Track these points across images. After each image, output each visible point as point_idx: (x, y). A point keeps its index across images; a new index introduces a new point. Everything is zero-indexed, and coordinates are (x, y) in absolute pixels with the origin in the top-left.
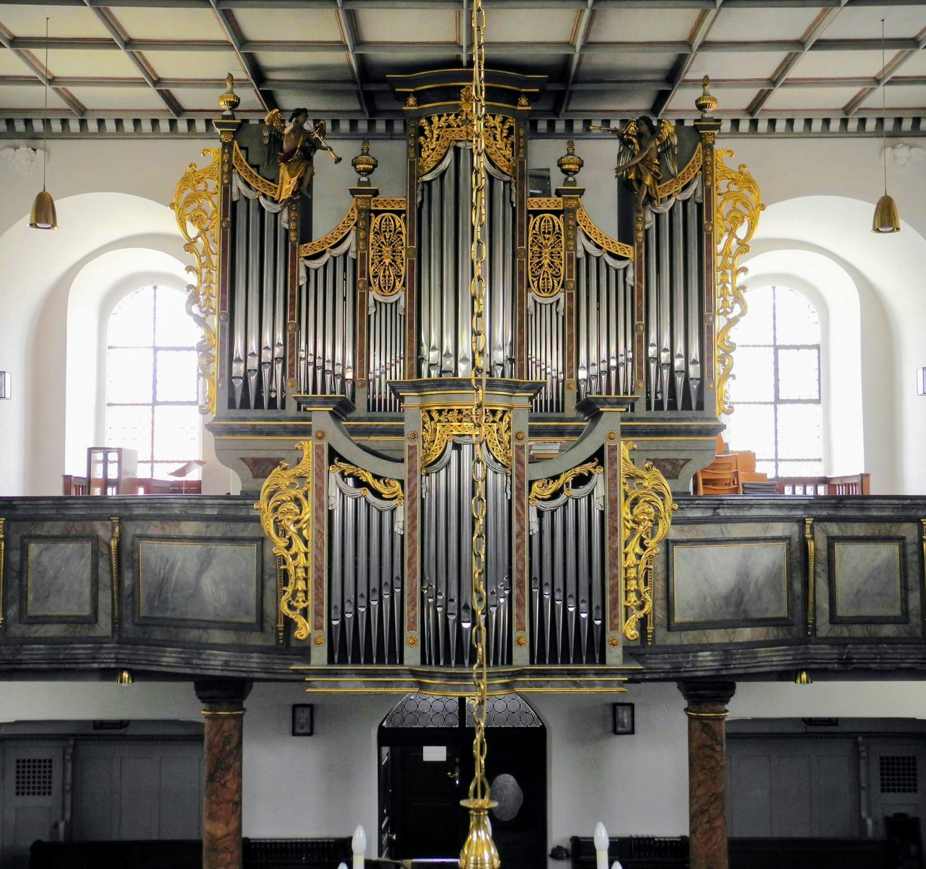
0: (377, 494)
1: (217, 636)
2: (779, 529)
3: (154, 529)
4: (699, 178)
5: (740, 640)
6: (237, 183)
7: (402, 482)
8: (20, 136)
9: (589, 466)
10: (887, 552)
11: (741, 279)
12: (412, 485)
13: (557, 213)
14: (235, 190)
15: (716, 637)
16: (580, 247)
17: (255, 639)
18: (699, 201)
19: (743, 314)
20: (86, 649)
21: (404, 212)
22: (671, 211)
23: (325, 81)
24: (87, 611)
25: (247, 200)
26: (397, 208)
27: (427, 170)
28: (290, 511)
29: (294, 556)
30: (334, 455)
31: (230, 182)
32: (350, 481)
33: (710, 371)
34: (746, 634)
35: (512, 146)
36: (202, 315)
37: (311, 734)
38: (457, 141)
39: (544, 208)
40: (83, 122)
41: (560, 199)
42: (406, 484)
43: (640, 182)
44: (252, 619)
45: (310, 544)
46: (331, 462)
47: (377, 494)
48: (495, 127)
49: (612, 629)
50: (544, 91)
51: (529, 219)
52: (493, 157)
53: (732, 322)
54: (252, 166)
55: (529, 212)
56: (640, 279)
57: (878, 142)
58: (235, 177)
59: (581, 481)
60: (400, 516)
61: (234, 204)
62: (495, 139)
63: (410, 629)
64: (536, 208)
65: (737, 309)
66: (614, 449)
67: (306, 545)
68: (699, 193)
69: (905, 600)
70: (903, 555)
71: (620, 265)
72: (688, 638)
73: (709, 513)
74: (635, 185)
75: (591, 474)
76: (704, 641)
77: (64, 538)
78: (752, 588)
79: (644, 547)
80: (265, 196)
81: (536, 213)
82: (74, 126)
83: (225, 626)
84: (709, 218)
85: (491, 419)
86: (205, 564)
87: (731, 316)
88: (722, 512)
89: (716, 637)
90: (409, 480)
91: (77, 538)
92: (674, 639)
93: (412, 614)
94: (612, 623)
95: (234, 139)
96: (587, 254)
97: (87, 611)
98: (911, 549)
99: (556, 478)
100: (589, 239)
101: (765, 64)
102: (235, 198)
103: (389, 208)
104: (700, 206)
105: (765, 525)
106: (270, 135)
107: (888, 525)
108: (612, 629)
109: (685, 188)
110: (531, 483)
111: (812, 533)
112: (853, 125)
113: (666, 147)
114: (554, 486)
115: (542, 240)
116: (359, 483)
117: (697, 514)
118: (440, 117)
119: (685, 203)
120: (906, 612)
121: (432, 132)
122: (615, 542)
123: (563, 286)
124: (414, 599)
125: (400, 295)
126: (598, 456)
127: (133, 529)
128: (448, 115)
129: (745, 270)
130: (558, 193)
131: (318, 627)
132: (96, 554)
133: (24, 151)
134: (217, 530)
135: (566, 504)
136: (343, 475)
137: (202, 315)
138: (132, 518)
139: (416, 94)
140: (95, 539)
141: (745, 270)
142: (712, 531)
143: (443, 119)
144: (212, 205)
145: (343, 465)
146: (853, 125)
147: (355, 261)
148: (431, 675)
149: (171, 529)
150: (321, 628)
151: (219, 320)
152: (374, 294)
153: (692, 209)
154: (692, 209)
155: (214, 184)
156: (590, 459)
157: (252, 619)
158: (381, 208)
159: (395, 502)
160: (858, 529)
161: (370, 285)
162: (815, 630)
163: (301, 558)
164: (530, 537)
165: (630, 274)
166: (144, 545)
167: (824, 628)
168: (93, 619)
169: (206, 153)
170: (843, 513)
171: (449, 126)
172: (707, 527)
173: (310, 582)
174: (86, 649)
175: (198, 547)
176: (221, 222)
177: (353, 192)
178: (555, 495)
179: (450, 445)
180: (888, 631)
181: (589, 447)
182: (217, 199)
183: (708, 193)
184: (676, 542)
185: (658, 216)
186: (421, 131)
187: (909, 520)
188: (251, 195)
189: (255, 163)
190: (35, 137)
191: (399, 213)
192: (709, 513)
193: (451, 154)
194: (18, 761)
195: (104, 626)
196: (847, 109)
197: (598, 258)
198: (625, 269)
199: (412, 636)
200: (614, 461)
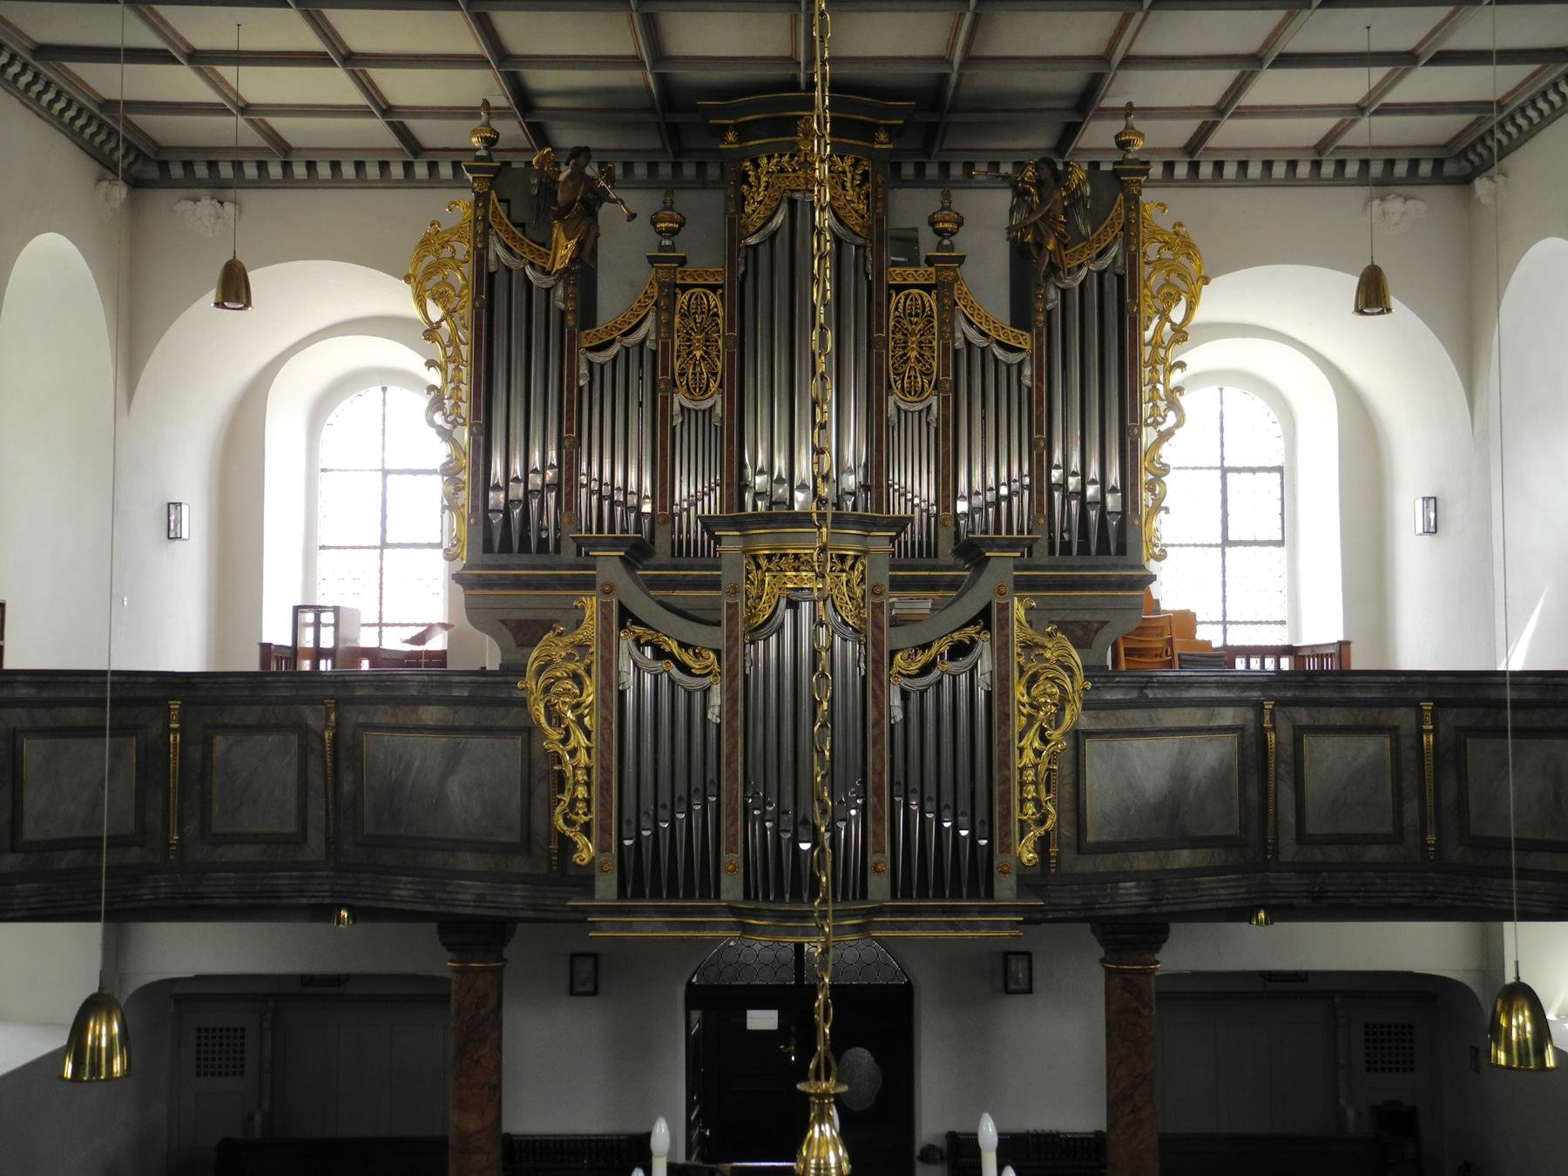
0: (685, 668)
1: (469, 861)
2: (1227, 716)
3: (382, 716)
4: (1120, 240)
5: (1176, 867)
6: (496, 249)
7: (718, 652)
8: (201, 184)
9: (971, 631)
10: (1373, 747)
11: (1176, 377)
12: (732, 656)
13: (928, 288)
14: (492, 257)
15: (1143, 861)
16: (958, 335)
17: (519, 865)
18: (1119, 272)
19: (1179, 424)
20: (291, 878)
21: (721, 286)
22: (1082, 285)
23: (614, 110)
24: (291, 827)
25: (509, 270)
26: (711, 281)
27: (752, 229)
28: (567, 692)
29: (573, 753)
30: (626, 617)
31: (486, 246)
32: (648, 651)
33: (1135, 502)
34: (1184, 858)
35: (867, 198)
36: (448, 427)
37: (595, 993)
38: (793, 191)
39: (910, 281)
40: (287, 166)
41: (931, 269)
42: (724, 655)
43: (1040, 246)
44: (514, 837)
45: (593, 736)
46: (622, 626)
47: (685, 668)
48: (844, 172)
49: (1002, 852)
50: (909, 124)
51: (890, 296)
52: (841, 213)
53: (1164, 436)
54: (516, 225)
55: (891, 287)
56: (1040, 379)
57: (1362, 192)
58: (493, 239)
59: (959, 650)
60: (716, 699)
61: (491, 276)
62: (844, 188)
63: (729, 851)
64: (899, 281)
65: (1171, 418)
66: (1005, 608)
67: (589, 738)
68: (1120, 261)
69: (1398, 812)
70: (1396, 750)
71: (1014, 358)
72: (1106, 863)
73: (1134, 694)
74: (1033, 251)
75: (973, 642)
76: (1127, 867)
77: (261, 728)
78: (1191, 795)
79: (1045, 741)
80: (532, 265)
81: (899, 288)
82: (275, 171)
83: (478, 847)
84: (1134, 296)
85: (839, 567)
86: (452, 762)
87: (1162, 428)
88: (1150, 694)
89: (1143, 861)
90: (729, 650)
91: (279, 728)
92: (1086, 865)
93: (732, 831)
94: (1001, 844)
95: (490, 188)
96: (968, 344)
97: (291, 827)
98: (1407, 742)
99: (926, 646)
100: (971, 323)
101: (1208, 87)
102: (493, 268)
103: (700, 281)
104: (1121, 278)
105: (1208, 711)
106: (540, 182)
107: (1375, 711)
108: (1002, 852)
109: (1100, 255)
110: (893, 653)
111: (1273, 721)
112: (1328, 170)
113: (1076, 199)
114: (923, 658)
115: (907, 325)
116: (660, 654)
117: (1117, 695)
118: (770, 158)
119: (1101, 274)
120: (1399, 828)
121: (758, 178)
122: (1006, 733)
123: (935, 388)
124: (734, 810)
125: (715, 401)
126: (984, 618)
127: (355, 716)
128: (781, 156)
129: (1181, 365)
130: (930, 261)
131: (603, 848)
132: (304, 750)
133: (206, 206)
134: (467, 717)
135: (939, 682)
136: (639, 644)
137: (448, 427)
138: (353, 701)
139: (736, 127)
140: (302, 729)
141: (1181, 365)
142: (1138, 718)
143: (774, 161)
144: (460, 277)
145: (639, 630)
146: (1328, 170)
147: (654, 353)
148: (757, 914)
149: (404, 716)
150: (609, 849)
151: (471, 433)
152: (680, 398)
153: (1111, 284)
154: (1111, 284)
155: (463, 249)
156: (972, 622)
157: (514, 837)
158: (690, 281)
159: (708, 680)
160: (1336, 716)
161: (675, 385)
162: (1276, 852)
163: (582, 757)
164: (892, 727)
165: (1027, 371)
166: (369, 738)
167: (1288, 850)
168: (300, 838)
169: (453, 207)
170: (1314, 694)
171: (782, 170)
172: (1130, 714)
173: (593, 788)
174: (291, 878)
175: (443, 740)
176: (474, 301)
177: (652, 260)
178: (925, 670)
179: (783, 603)
180: (1376, 853)
181: (971, 604)
182: (467, 269)
183: (1132, 262)
184: (1090, 734)
185: (1064, 292)
186: (744, 177)
187: (1404, 703)
188: (514, 264)
189: (520, 221)
190: (223, 185)
191: (714, 288)
192: (1134, 694)
193: (784, 207)
194: (199, 1030)
195: (316, 846)
196: (1321, 147)
197: (983, 350)
198: (1020, 365)
199: (732, 860)
200: (1005, 623)
